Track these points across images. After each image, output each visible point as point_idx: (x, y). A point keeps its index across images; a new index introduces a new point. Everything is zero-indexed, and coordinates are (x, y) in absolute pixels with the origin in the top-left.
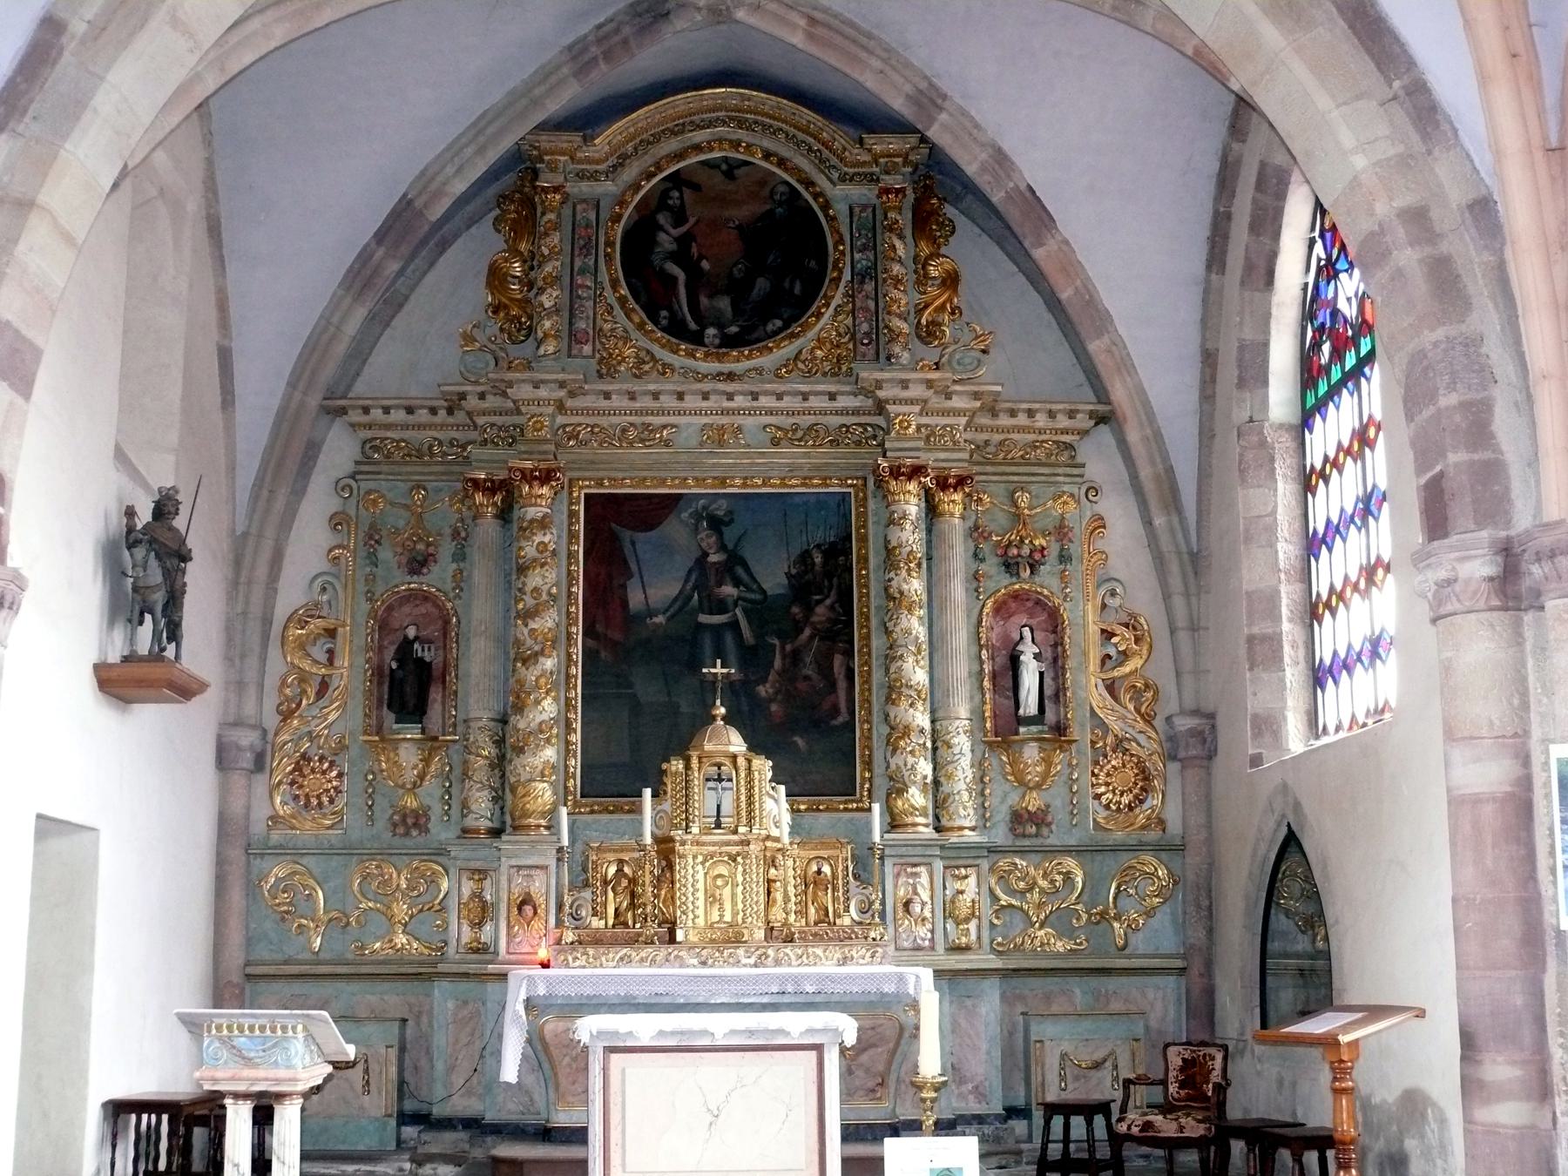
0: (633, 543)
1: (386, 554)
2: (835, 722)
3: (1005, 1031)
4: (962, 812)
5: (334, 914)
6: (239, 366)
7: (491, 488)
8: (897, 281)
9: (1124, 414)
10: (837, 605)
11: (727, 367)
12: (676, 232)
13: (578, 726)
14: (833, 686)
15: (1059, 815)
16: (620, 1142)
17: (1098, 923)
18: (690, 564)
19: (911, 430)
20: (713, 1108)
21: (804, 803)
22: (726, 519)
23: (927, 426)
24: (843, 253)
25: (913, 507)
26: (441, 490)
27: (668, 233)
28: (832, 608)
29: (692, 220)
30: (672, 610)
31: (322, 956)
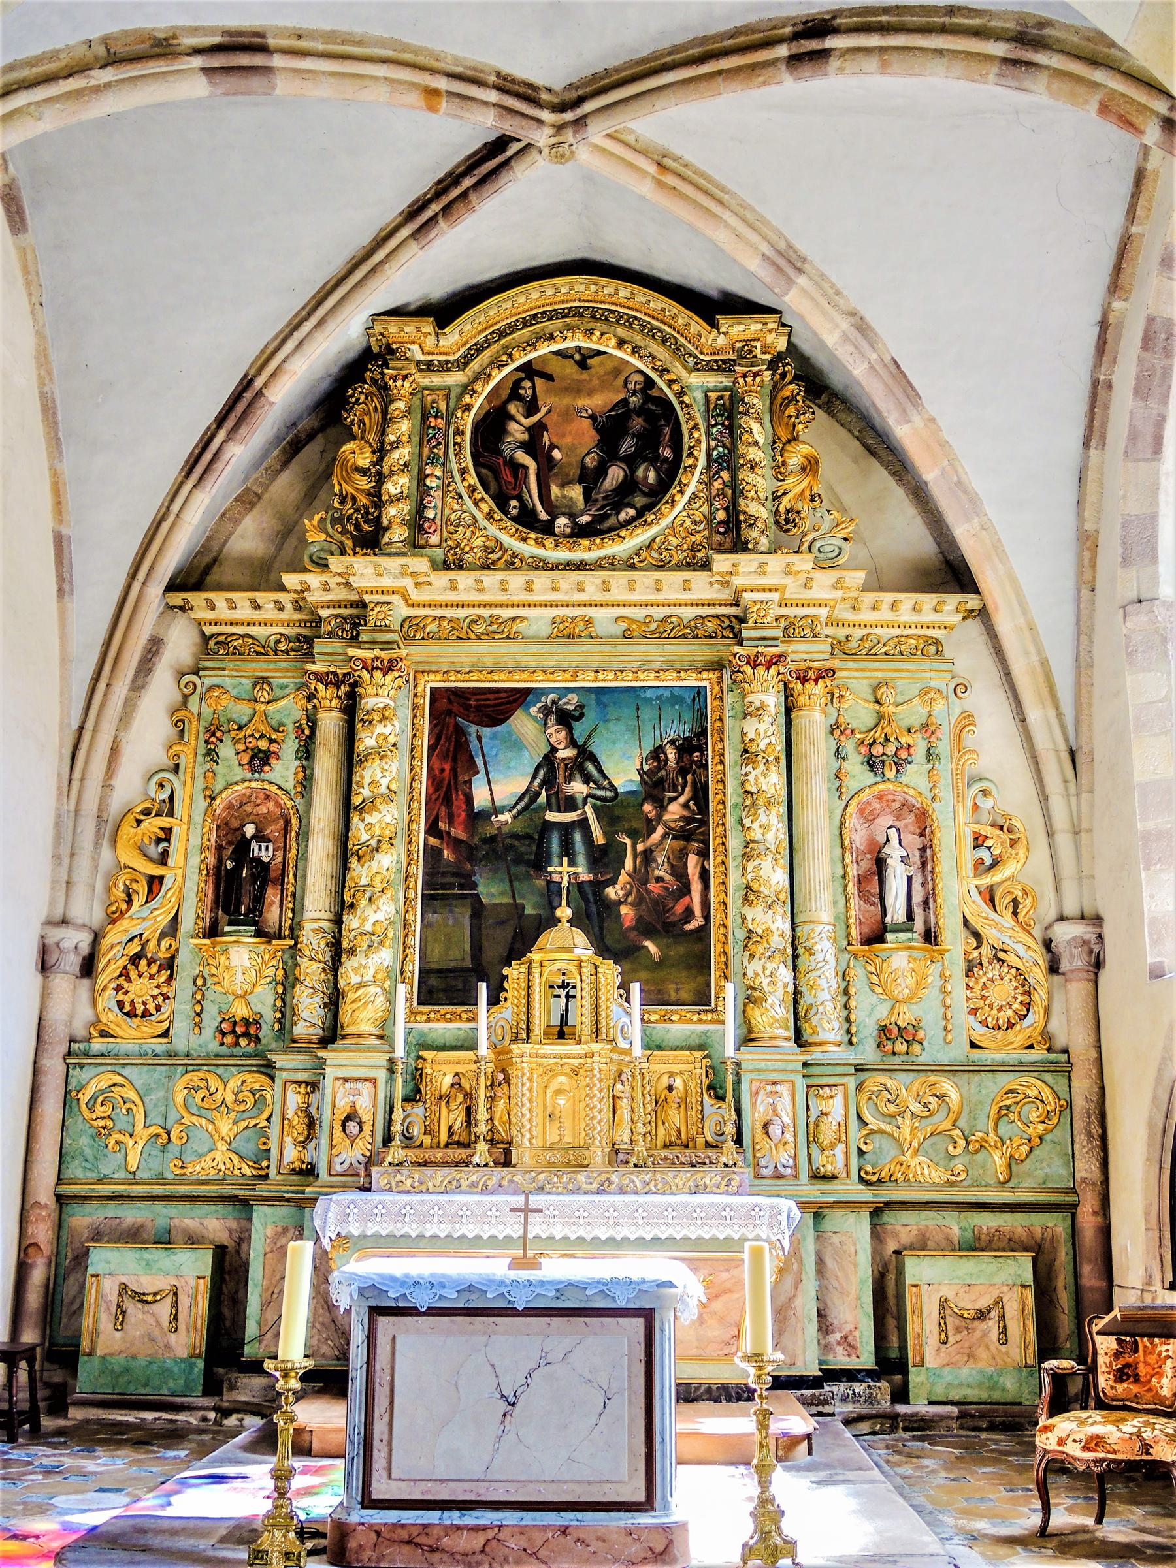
0: (479, 738)
1: (226, 750)
2: (688, 927)
3: (876, 1272)
4: (827, 1026)
5: (154, 1130)
6: (78, 558)
7: (332, 680)
8: (753, 466)
9: (995, 603)
10: (691, 803)
11: (577, 555)
12: (528, 422)
13: (417, 928)
14: (685, 890)
15: (931, 1031)
16: (386, 1437)
17: (976, 1152)
18: (539, 759)
19: (769, 619)
20: (508, 1393)
21: (655, 1013)
22: (577, 714)
23: (787, 617)
24: (699, 441)
25: (772, 700)
26: (286, 687)
27: (518, 422)
28: (686, 806)
29: (544, 410)
30: (519, 807)
31: (139, 1174)
